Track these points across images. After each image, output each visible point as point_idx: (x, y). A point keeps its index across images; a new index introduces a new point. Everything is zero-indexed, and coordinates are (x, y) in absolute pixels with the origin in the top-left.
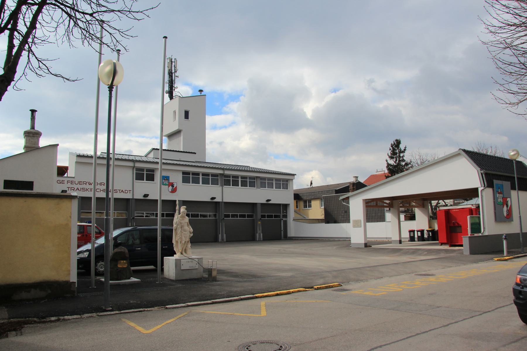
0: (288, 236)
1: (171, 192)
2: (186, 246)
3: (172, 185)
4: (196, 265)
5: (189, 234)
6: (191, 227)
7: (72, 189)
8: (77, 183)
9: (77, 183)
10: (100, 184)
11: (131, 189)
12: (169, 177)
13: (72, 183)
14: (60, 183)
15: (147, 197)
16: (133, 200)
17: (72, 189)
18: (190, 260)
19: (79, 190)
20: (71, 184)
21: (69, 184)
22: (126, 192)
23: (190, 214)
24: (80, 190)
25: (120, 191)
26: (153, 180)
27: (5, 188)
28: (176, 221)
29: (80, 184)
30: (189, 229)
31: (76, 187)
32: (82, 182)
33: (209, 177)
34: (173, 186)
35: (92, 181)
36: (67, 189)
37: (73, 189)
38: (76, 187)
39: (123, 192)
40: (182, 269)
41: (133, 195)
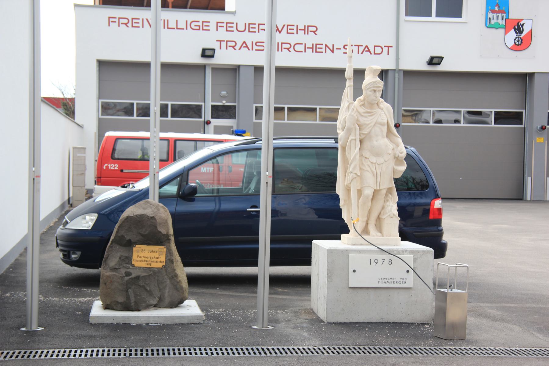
2: (383, 208)
4: (406, 275)
5: (392, 164)
6: (400, 140)
7: (229, 44)
8: (241, 28)
9: (241, 28)
10: (304, 30)
11: (392, 43)
13: (229, 29)
14: (198, 28)
15: (439, 64)
16: (397, 75)
17: (229, 44)
18: (387, 256)
19: (247, 47)
20: (227, 31)
21: (222, 30)
24: (250, 48)
25: (361, 49)
26: (459, 15)
28: (345, 119)
29: (251, 30)
30: (391, 146)
31: (239, 38)
32: (256, 26)
34: (519, 29)
35: (265, 19)
36: (216, 46)
37: (233, 44)
38: (239, 38)
39: (369, 51)
40: (350, 286)
41: (397, 59)
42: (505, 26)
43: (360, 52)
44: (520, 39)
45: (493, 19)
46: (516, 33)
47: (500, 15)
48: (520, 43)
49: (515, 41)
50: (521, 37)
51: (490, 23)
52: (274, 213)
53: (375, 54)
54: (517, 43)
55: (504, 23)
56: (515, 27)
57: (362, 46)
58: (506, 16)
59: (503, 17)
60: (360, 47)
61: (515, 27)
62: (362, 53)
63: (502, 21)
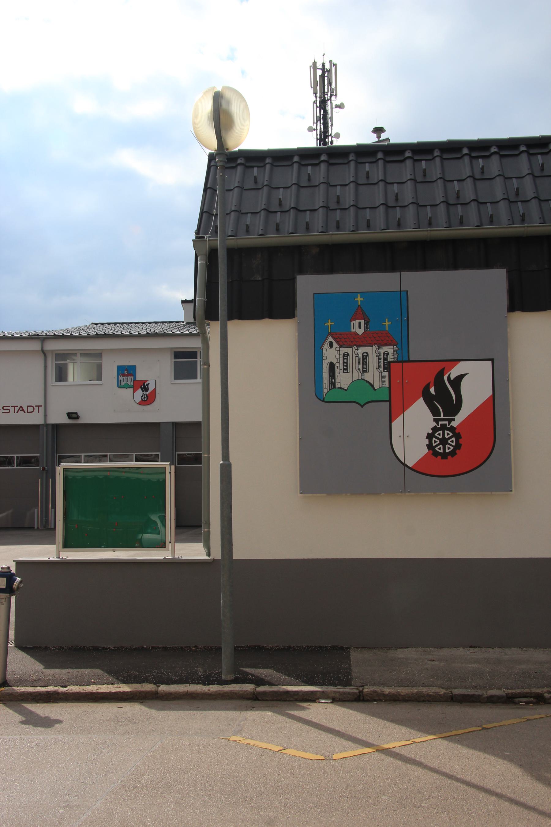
0: (202, 544)
1: (140, 404)
3: (143, 386)
11: (41, 403)
12: (134, 368)
22: (30, 409)
23: (14, 457)
25: (17, 409)
27: (451, 425)
33: (197, 358)
34: (145, 388)
39: (23, 410)
42: (133, 386)
43: (16, 411)
44: (448, 434)
45: (346, 369)
46: (143, 391)
47: (371, 351)
48: (146, 399)
49: (430, 442)
50: (454, 424)
51: (332, 385)
52: (8, 456)
53: (28, 412)
54: (440, 449)
55: (132, 384)
56: (141, 387)
57: (17, 406)
58: (134, 378)
59: (131, 379)
60: (16, 407)
61: (427, 388)
62: (17, 412)
63: (131, 383)
